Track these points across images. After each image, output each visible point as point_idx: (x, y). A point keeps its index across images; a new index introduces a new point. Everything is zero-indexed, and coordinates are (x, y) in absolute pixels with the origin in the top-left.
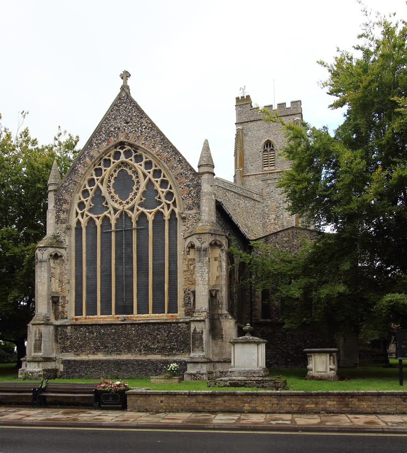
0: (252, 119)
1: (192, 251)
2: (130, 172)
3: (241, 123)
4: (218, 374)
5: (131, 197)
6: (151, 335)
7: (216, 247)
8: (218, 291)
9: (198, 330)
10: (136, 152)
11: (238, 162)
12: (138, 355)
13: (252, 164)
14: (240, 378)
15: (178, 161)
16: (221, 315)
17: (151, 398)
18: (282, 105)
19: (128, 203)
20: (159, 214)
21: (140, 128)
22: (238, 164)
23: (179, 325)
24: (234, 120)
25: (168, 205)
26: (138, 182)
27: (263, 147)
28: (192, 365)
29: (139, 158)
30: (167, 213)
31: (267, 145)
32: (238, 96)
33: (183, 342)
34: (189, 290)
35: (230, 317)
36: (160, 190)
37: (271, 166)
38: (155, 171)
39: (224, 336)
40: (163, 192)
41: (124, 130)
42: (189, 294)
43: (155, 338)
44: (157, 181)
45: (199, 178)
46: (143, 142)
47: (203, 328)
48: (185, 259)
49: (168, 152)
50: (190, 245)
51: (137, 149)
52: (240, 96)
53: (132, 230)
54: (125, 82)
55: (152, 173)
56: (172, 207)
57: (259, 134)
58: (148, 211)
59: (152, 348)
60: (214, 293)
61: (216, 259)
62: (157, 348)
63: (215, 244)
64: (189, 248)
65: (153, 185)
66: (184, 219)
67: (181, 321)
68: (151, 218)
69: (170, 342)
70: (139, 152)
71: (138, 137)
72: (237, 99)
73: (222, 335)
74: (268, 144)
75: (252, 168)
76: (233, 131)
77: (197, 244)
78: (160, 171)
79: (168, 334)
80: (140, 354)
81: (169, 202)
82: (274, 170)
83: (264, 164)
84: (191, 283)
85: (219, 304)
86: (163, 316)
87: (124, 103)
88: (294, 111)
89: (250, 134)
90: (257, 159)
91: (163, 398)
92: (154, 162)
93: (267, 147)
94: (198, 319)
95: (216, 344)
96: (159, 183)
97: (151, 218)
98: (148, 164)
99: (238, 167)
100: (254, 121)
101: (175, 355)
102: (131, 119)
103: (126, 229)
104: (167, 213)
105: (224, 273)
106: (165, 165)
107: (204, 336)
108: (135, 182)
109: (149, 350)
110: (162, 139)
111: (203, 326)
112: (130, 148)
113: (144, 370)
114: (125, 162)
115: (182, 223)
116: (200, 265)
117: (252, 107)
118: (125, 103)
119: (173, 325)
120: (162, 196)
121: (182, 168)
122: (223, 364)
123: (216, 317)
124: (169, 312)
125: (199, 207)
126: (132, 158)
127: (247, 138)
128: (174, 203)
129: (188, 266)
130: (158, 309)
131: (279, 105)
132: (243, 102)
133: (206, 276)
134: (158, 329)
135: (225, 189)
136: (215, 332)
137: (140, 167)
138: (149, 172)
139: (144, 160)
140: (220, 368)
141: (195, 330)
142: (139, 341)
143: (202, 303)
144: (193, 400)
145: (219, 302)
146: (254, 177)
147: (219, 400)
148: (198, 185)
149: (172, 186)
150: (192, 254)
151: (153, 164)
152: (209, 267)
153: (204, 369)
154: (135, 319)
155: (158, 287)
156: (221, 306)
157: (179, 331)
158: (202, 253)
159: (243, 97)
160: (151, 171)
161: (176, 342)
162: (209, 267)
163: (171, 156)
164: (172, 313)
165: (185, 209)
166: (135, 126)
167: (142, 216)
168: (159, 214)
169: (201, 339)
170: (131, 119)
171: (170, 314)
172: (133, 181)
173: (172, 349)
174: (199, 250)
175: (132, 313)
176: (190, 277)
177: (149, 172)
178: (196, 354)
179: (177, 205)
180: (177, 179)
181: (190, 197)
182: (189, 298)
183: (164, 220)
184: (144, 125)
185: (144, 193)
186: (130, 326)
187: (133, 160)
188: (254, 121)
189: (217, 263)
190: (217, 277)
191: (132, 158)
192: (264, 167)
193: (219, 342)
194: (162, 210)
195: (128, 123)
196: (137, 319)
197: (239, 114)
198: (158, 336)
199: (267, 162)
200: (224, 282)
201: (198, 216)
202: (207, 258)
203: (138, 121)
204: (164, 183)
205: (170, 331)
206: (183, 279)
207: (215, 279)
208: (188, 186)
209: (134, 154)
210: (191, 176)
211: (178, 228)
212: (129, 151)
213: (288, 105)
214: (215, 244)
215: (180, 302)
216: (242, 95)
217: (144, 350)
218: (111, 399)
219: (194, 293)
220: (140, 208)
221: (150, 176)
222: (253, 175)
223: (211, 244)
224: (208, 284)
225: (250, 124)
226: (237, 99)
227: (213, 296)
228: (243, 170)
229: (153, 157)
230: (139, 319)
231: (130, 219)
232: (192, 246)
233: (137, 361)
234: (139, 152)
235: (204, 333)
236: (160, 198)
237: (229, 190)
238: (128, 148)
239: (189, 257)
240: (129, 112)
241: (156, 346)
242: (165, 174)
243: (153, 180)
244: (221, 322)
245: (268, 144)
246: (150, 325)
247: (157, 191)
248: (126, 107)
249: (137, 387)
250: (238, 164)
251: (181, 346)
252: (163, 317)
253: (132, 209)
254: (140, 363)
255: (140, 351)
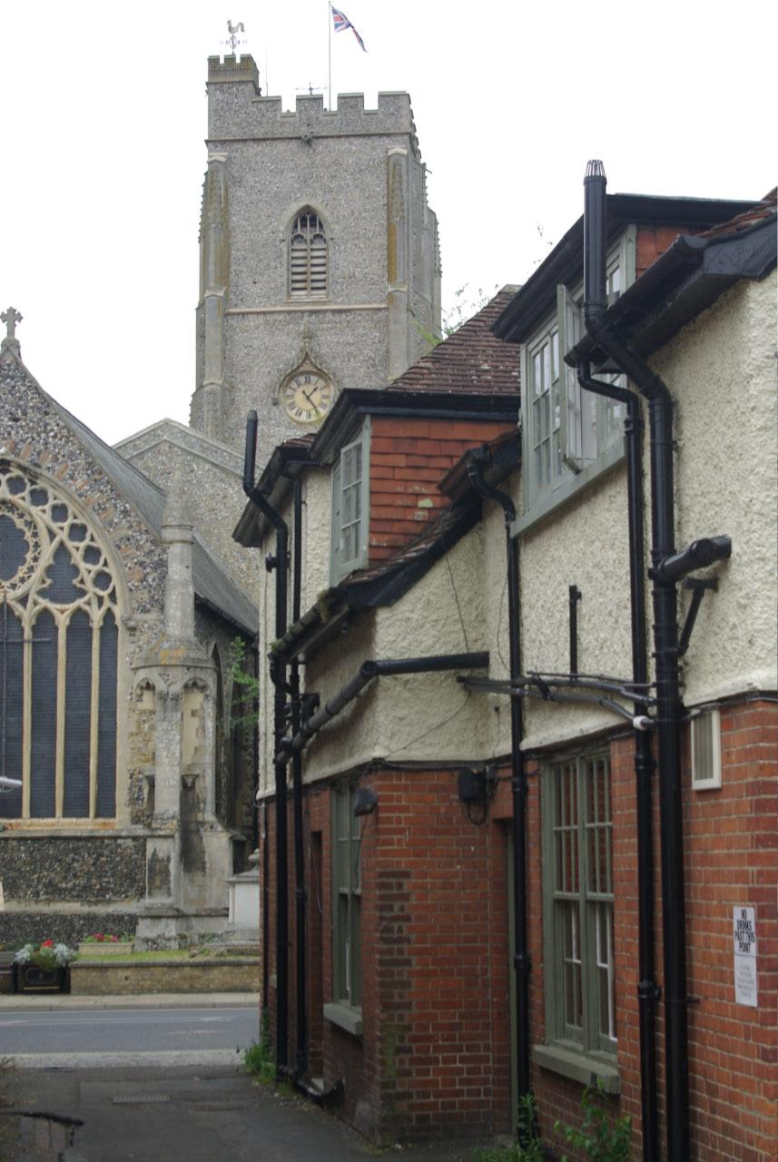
0: (258, 132)
1: (147, 696)
2: (19, 523)
3: (223, 142)
4: (196, 939)
5: (20, 574)
6: (60, 861)
7: (195, 690)
8: (197, 776)
9: (161, 855)
10: (33, 483)
11: (211, 267)
12: (33, 903)
13: (257, 278)
14: (243, 942)
15: (123, 512)
16: (203, 823)
17: (109, 973)
18: (351, 102)
19: (14, 586)
20: (80, 617)
21: (43, 435)
22: (212, 276)
23: (119, 841)
24: (200, 127)
25: (100, 600)
26: (37, 545)
27: (292, 225)
28: (148, 921)
29: (39, 497)
30: (97, 616)
31: (304, 220)
32: (214, 53)
33: (128, 876)
34: (140, 772)
35: (220, 828)
36: (83, 566)
37: (313, 289)
38: (73, 527)
39: (208, 865)
40: (89, 572)
41: (9, 433)
42: (139, 780)
43: (69, 868)
44: (78, 549)
45: (164, 551)
46: (50, 465)
47: (167, 849)
48: (134, 711)
49: (102, 491)
50: (144, 684)
51: (37, 478)
52: (222, 52)
53: (21, 644)
54: (11, 331)
55: (66, 530)
56: (107, 603)
57: (280, 183)
58: (59, 606)
59: (62, 889)
60: (189, 781)
61: (194, 714)
62: (73, 889)
63: (195, 684)
64: (142, 688)
65: (69, 556)
66: (132, 630)
67: (124, 834)
68: (62, 621)
69: (101, 877)
70: (41, 484)
71: (39, 453)
72: (213, 61)
73: (204, 863)
74: (307, 218)
75: (255, 289)
76: (197, 161)
77: (161, 686)
78: (84, 528)
79: (97, 859)
80: (37, 902)
81: (101, 593)
82: (324, 303)
83: (294, 281)
84: (143, 758)
85: (199, 803)
86: (86, 824)
87: (8, 376)
88: (389, 125)
89: (250, 179)
90: (273, 264)
91: (128, 973)
92: (71, 509)
93: (304, 225)
94: (162, 833)
95: (192, 881)
96: (81, 552)
97: (62, 621)
98: (60, 512)
99: (212, 284)
100: (265, 140)
101: (109, 902)
102: (25, 414)
103: (10, 640)
104: (97, 616)
105: (210, 741)
106: (97, 517)
107: (173, 867)
108: (31, 544)
109: (55, 892)
110: (89, 464)
111: (172, 846)
112: (20, 473)
113: (72, 930)
114: (10, 502)
115: (128, 638)
116: (165, 727)
117: (258, 91)
118: (12, 378)
119: (106, 841)
120: (89, 579)
121: (131, 527)
122: (206, 919)
123: (193, 827)
124: (97, 815)
125: (162, 608)
126: (26, 494)
127: (240, 193)
128: (113, 596)
129: (140, 723)
130: (75, 806)
131: (343, 99)
132: (232, 77)
133: (176, 748)
134: (76, 851)
135: (190, 453)
136: (191, 857)
137: (41, 515)
138: (62, 529)
139: (51, 502)
140: (199, 927)
141: (154, 854)
142: (35, 872)
143: (168, 801)
144: (177, 975)
145: (198, 798)
146: (261, 319)
147: (215, 973)
148: (162, 565)
149: (108, 561)
150: (148, 701)
151: (70, 512)
152: (182, 730)
153: (171, 928)
154: (25, 828)
155: (76, 763)
156: (202, 805)
157: (117, 854)
158: (169, 703)
159: (230, 59)
160: (66, 525)
161: (113, 875)
162: (182, 730)
163: (108, 500)
164: (103, 816)
165: (133, 610)
166: (33, 428)
167: (45, 618)
168: (80, 617)
169: (167, 872)
170: (25, 414)
171: (100, 820)
172: (27, 543)
173: (104, 890)
174: (163, 697)
175: (18, 815)
176: (141, 745)
177: (62, 529)
178: (158, 900)
179: (119, 601)
180: (119, 548)
181: (145, 588)
182: (140, 789)
183: (91, 630)
184: (52, 430)
185: (49, 571)
186: (15, 843)
187: (28, 499)
188: (265, 140)
189: (196, 722)
190: (196, 749)
191: (26, 494)
192: (294, 289)
193: (198, 876)
194: (86, 608)
195: (16, 420)
196: (31, 828)
197: (216, 113)
198: (75, 865)
199: (305, 273)
200: (208, 759)
201: (161, 626)
202: (179, 714)
203: (40, 420)
204: (92, 554)
205: (101, 855)
206: (129, 750)
207: (192, 752)
208: (141, 564)
209: (29, 488)
210: (148, 544)
211: (120, 647)
212: (19, 479)
213: (371, 104)
214: (195, 684)
215: (122, 794)
216: (229, 52)
217: (46, 893)
218: (41, 976)
219: (152, 782)
220: (40, 600)
221: (63, 536)
222: (258, 313)
223: (186, 686)
224: (180, 764)
225: (253, 149)
226: (213, 61)
227: (187, 786)
228: (226, 294)
229: (71, 497)
230: (35, 828)
231: (19, 620)
232: (149, 687)
233: (31, 916)
234: (41, 484)
235: (172, 861)
236: (82, 581)
237: (199, 457)
238: (15, 472)
239: (141, 706)
240: (20, 399)
241: (70, 885)
242: (95, 536)
243: (70, 545)
244: (201, 838)
245: (307, 218)
246: (58, 842)
247: (76, 570)
248: (14, 387)
249: (91, 951)
250: (212, 276)
251: (121, 885)
252: (86, 825)
253: (23, 600)
254: (38, 918)
255: (37, 894)
